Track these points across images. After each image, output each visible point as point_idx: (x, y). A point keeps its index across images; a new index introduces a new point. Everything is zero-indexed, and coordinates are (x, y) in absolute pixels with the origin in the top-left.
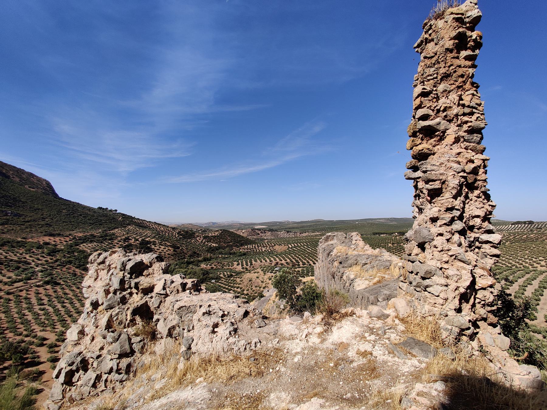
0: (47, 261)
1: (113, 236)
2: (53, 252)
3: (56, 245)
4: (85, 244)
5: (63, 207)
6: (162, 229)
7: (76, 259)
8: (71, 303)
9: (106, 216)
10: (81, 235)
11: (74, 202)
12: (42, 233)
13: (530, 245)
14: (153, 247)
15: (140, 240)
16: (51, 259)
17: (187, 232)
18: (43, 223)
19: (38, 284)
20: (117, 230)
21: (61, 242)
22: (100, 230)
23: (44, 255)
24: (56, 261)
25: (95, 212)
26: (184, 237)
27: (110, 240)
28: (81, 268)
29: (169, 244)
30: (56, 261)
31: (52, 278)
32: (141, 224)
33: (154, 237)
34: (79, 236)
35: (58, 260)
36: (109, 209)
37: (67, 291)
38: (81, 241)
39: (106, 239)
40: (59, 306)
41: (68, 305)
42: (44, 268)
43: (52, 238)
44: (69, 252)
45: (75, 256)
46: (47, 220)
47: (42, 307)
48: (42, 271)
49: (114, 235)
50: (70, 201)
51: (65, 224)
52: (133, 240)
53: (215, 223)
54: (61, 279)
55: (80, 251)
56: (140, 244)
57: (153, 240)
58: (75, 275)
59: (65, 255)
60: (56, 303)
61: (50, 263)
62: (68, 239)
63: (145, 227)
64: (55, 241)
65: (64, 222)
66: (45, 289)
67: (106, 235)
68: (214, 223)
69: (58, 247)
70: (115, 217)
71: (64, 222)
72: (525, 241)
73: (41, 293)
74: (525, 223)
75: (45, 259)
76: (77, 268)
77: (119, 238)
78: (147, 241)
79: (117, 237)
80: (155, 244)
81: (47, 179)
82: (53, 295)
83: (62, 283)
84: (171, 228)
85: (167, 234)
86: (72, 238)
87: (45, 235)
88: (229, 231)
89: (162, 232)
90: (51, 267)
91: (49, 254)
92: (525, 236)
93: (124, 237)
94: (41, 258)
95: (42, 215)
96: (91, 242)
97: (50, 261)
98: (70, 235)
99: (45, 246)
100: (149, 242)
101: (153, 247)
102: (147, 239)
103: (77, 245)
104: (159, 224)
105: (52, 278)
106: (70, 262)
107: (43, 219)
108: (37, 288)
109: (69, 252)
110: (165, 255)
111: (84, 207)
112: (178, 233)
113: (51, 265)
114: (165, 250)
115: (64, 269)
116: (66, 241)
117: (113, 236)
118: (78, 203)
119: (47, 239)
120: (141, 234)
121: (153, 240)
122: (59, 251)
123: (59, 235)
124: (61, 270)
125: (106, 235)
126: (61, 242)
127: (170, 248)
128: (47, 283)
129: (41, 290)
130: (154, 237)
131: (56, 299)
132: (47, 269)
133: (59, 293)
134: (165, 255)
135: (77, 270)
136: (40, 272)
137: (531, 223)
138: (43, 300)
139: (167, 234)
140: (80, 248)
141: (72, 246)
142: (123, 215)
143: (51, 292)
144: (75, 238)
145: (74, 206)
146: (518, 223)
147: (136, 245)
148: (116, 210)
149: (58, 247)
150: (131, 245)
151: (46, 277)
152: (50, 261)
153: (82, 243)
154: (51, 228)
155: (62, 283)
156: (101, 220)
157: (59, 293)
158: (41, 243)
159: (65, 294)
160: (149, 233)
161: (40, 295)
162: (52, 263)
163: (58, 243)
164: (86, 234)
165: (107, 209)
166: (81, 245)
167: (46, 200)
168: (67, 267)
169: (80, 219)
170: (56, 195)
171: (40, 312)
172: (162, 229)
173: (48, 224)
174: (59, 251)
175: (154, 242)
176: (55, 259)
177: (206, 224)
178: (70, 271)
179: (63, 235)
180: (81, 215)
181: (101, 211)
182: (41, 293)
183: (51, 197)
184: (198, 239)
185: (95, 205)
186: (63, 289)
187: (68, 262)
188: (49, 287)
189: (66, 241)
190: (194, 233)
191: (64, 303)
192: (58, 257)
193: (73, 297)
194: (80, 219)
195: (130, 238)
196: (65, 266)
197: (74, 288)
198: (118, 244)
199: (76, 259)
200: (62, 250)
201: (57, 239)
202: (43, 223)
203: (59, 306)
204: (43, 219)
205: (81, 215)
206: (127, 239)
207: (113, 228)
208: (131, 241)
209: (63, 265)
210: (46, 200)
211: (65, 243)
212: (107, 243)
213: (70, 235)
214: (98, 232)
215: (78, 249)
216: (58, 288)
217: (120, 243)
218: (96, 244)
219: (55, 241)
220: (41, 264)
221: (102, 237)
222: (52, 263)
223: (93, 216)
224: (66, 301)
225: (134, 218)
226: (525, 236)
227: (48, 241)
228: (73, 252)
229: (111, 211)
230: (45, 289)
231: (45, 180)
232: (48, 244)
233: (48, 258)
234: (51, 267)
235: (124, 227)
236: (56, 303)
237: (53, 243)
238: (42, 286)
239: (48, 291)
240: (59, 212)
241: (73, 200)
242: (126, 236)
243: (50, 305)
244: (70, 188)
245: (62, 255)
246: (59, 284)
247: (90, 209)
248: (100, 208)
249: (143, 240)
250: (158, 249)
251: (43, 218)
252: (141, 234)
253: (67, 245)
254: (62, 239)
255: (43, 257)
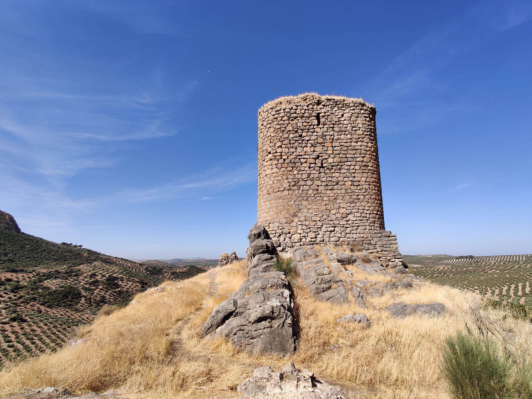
0: (10, 298)
1: (79, 272)
2: (16, 289)
3: (18, 282)
4: (49, 281)
5: (26, 242)
6: (129, 265)
7: (40, 296)
8: (40, 339)
9: (71, 251)
10: (45, 271)
11: (36, 238)
12: (4, 269)
13: (468, 276)
14: (120, 283)
15: (107, 276)
16: (15, 296)
17: (154, 268)
18: (5, 258)
19: (4, 321)
20: (82, 266)
21: (23, 279)
22: (65, 266)
23: (6, 291)
24: (20, 298)
25: (59, 248)
26: (152, 273)
27: (75, 276)
28: (46, 305)
29: (137, 280)
30: (20, 298)
31: (18, 315)
32: (108, 260)
33: (122, 273)
34: (43, 272)
35: (22, 296)
36: (74, 244)
37: (35, 328)
38: (45, 278)
39: (71, 275)
40: (28, 343)
41: (38, 342)
42: (7, 305)
43: (14, 274)
44: (32, 289)
45: (39, 293)
46: (9, 255)
47: (11, 344)
48: (5, 309)
49: (80, 271)
50: (33, 237)
51: (28, 259)
52: (100, 276)
53: (180, 260)
54: (26, 315)
55: (45, 288)
56: (107, 280)
57: (121, 276)
58: (40, 312)
59: (28, 292)
60: (24, 340)
61: (13, 300)
62: (31, 275)
63: (112, 263)
64: (17, 278)
65: (27, 258)
66: (12, 326)
67: (72, 271)
68: (179, 260)
69: (21, 283)
70: (80, 253)
71: (27, 258)
72: (465, 273)
73: (7, 331)
74: (466, 257)
75: (8, 296)
76: (42, 305)
77: (85, 275)
78: (115, 277)
79: (82, 273)
80: (123, 280)
81: (10, 214)
82: (20, 331)
83: (29, 320)
84: (138, 264)
85: (134, 270)
86: (35, 274)
87: (7, 271)
88: (197, 268)
89: (129, 268)
90: (14, 304)
91: (12, 291)
92: (465, 269)
93: (90, 273)
94: (4, 295)
95: (5, 250)
96: (56, 278)
97: (13, 298)
98: (33, 271)
99: (8, 283)
100: (116, 278)
101: (120, 283)
102: (115, 275)
103: (41, 282)
104: (126, 260)
105: (18, 315)
106: (34, 299)
107: (6, 255)
108: (3, 325)
109: (32, 289)
110: (132, 291)
111: (48, 243)
112: (145, 269)
113: (14, 302)
114: (133, 286)
115: (28, 306)
116: (29, 278)
117: (79, 272)
118: (41, 239)
119: (9, 275)
120: (108, 270)
121: (121, 276)
122: (22, 288)
123: (22, 271)
124: (25, 308)
125: (72, 271)
126: (23, 279)
127: (138, 284)
128: (14, 320)
129: (7, 327)
130: (122, 273)
131: (23, 336)
132: (10, 307)
133: (27, 330)
134: (132, 291)
135: (42, 308)
136: (4, 309)
137: (471, 257)
138: (10, 337)
139: (134, 270)
140: (44, 285)
141: (35, 283)
142: (89, 250)
143: (17, 329)
144: (39, 274)
145: (38, 241)
146: (461, 257)
147: (103, 282)
148: (81, 246)
149: (21, 283)
150: (97, 281)
151: (12, 314)
152: (13, 298)
153: (46, 279)
154: (14, 264)
155: (29, 320)
156: (66, 256)
157: (27, 330)
158: (3, 280)
159: (33, 330)
160: (115, 268)
161: (6, 333)
162: (16, 300)
163: (21, 279)
164: (51, 270)
165: (71, 244)
166: (45, 282)
167: (9, 235)
168: (31, 304)
169: (44, 255)
170: (18, 230)
171: (9, 349)
172: (129, 265)
173: (10, 260)
174: (22, 288)
175: (122, 278)
176: (18, 296)
177: (171, 260)
178: (34, 308)
179: (26, 271)
180: (44, 251)
181: (65, 247)
182: (7, 331)
183: (13, 232)
184: (165, 275)
185: (58, 240)
186: (30, 325)
187: (33, 299)
188: (15, 324)
189: (29, 278)
190: (162, 269)
191: (32, 339)
192: (22, 293)
193: (42, 334)
194: (44, 255)
195: (97, 274)
196: (28, 303)
197: (41, 324)
198: (83, 280)
199: (40, 296)
200: (26, 287)
201: (20, 275)
202: (5, 258)
203: (28, 343)
204: (6, 255)
205: (44, 251)
206: (94, 275)
207: (78, 264)
208: (97, 278)
209: (26, 302)
210: (9, 235)
211: (28, 280)
212: (72, 280)
213: (33, 271)
214: (63, 268)
215: (42, 285)
216: (24, 325)
217: (86, 279)
218: (60, 280)
219: (17, 278)
220: (4, 302)
221: (67, 273)
222: (16, 300)
223: (58, 252)
224: (34, 338)
225: (99, 254)
226: (465, 269)
227: (10, 277)
228: (37, 289)
229: (75, 246)
230: (12, 326)
231: (9, 215)
232: (10, 280)
233: (12, 295)
234: (14, 304)
235: (90, 263)
236: (24, 340)
237: (16, 279)
238: (8, 323)
239: (14, 328)
240: (23, 247)
241: (35, 235)
242: (93, 272)
243: (18, 342)
244: (29, 226)
245: (26, 292)
246: (25, 321)
247: (54, 245)
248: (64, 244)
249: (110, 276)
250: (125, 286)
251: (5, 253)
252: (108, 270)
253: (30, 281)
254: (25, 275)
255: (6, 293)
